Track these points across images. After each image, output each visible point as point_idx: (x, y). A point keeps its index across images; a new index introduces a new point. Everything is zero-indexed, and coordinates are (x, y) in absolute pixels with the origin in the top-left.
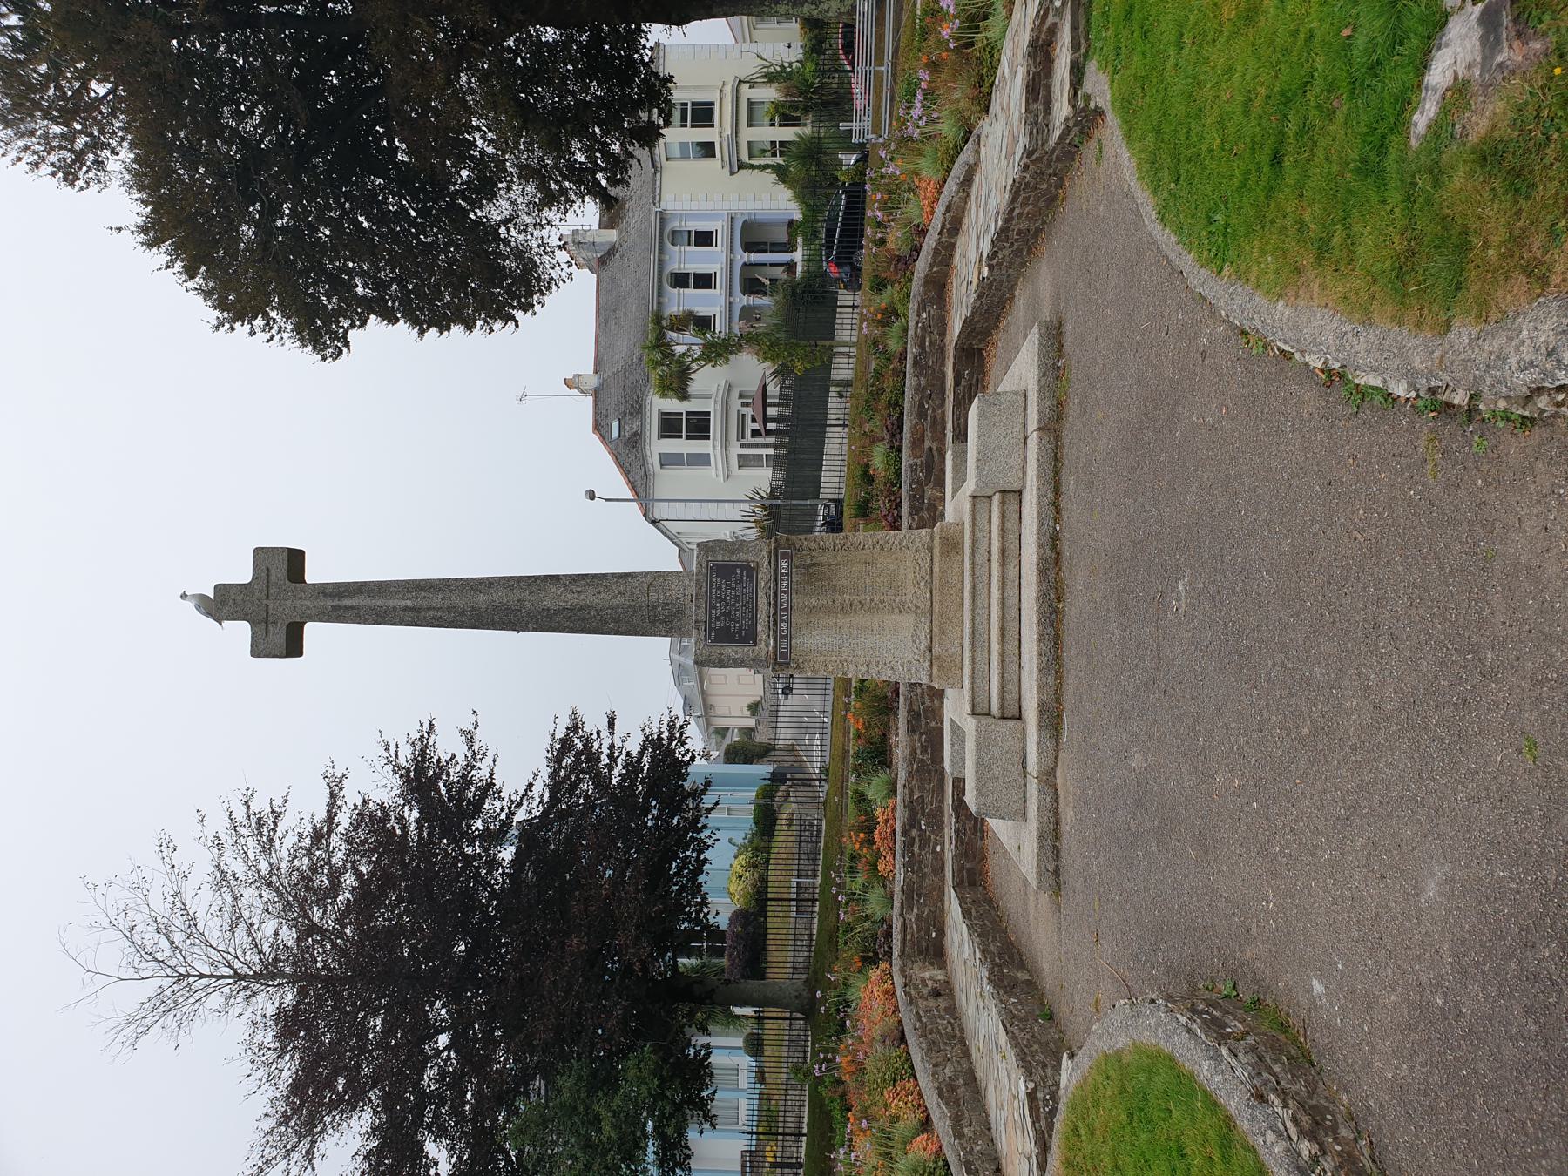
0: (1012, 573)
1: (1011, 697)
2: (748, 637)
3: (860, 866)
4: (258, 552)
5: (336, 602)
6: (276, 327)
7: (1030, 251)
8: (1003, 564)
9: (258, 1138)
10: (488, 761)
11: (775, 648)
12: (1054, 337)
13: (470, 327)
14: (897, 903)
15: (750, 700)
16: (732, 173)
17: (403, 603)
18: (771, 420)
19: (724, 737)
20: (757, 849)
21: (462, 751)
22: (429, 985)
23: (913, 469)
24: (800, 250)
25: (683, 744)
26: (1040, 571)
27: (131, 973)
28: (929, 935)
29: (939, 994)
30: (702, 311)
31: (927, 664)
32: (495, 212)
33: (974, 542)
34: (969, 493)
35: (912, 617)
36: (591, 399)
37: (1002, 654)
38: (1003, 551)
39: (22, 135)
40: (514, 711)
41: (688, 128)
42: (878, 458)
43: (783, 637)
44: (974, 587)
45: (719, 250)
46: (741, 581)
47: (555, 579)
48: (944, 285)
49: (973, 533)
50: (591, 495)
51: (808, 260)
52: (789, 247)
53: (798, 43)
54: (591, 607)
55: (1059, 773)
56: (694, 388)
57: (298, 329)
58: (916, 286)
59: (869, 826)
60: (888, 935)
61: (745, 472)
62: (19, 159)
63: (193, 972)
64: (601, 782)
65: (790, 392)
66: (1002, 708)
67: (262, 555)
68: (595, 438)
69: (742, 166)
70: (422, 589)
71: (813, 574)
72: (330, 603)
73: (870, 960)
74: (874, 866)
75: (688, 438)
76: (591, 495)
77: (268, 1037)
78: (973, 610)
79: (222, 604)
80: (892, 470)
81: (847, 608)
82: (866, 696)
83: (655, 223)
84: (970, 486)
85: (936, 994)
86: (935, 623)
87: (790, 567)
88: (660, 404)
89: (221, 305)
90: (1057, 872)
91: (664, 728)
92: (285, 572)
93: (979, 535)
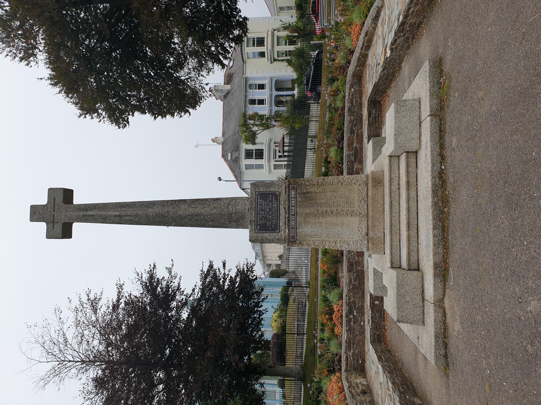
1: (414, 258)
2: (275, 228)
3: (326, 328)
4: (50, 190)
5: (85, 213)
6: (102, 117)
7: (413, 38)
11: (289, 234)
12: (438, 66)
13: (173, 115)
14: (343, 347)
15: (279, 254)
16: (271, 63)
17: (114, 213)
18: (286, 152)
19: (270, 267)
20: (282, 310)
21: (167, 275)
22: (157, 366)
23: (349, 156)
24: (296, 89)
25: (252, 273)
26: (433, 191)
27: (44, 359)
28: (358, 362)
29: (365, 393)
30: (261, 113)
31: (366, 242)
32: (182, 74)
33: (391, 179)
34: (388, 154)
35: (358, 218)
36: (221, 146)
37: (409, 237)
38: (408, 183)
39: (9, 47)
40: (190, 258)
41: (255, 47)
42: (333, 152)
43: (293, 228)
44: (391, 202)
45: (267, 90)
46: (272, 201)
47: (184, 201)
48: (361, 77)
49: (390, 174)
50: (220, 179)
51: (299, 92)
52: (293, 89)
53: (295, 16)
54: (201, 214)
55: (446, 301)
56: (257, 141)
57: (109, 117)
58: (349, 78)
59: (330, 312)
60: (340, 361)
61: (276, 171)
62: (7, 55)
63: (67, 359)
64: (221, 288)
65: (293, 141)
66: (409, 265)
67: (51, 191)
68: (223, 160)
69: (275, 60)
70: (123, 206)
71: (307, 197)
72: (81, 213)
73: (331, 371)
74: (332, 330)
75: (255, 159)
76: (220, 179)
77: (91, 387)
78: (391, 214)
79: (37, 213)
80: (339, 157)
81: (324, 214)
82: (328, 256)
83: (244, 81)
84: (388, 148)
85: (364, 393)
86: (370, 221)
87: (296, 194)
88: (245, 146)
89: (81, 108)
90: (446, 356)
91: (245, 266)
92: (62, 199)
93: (393, 176)
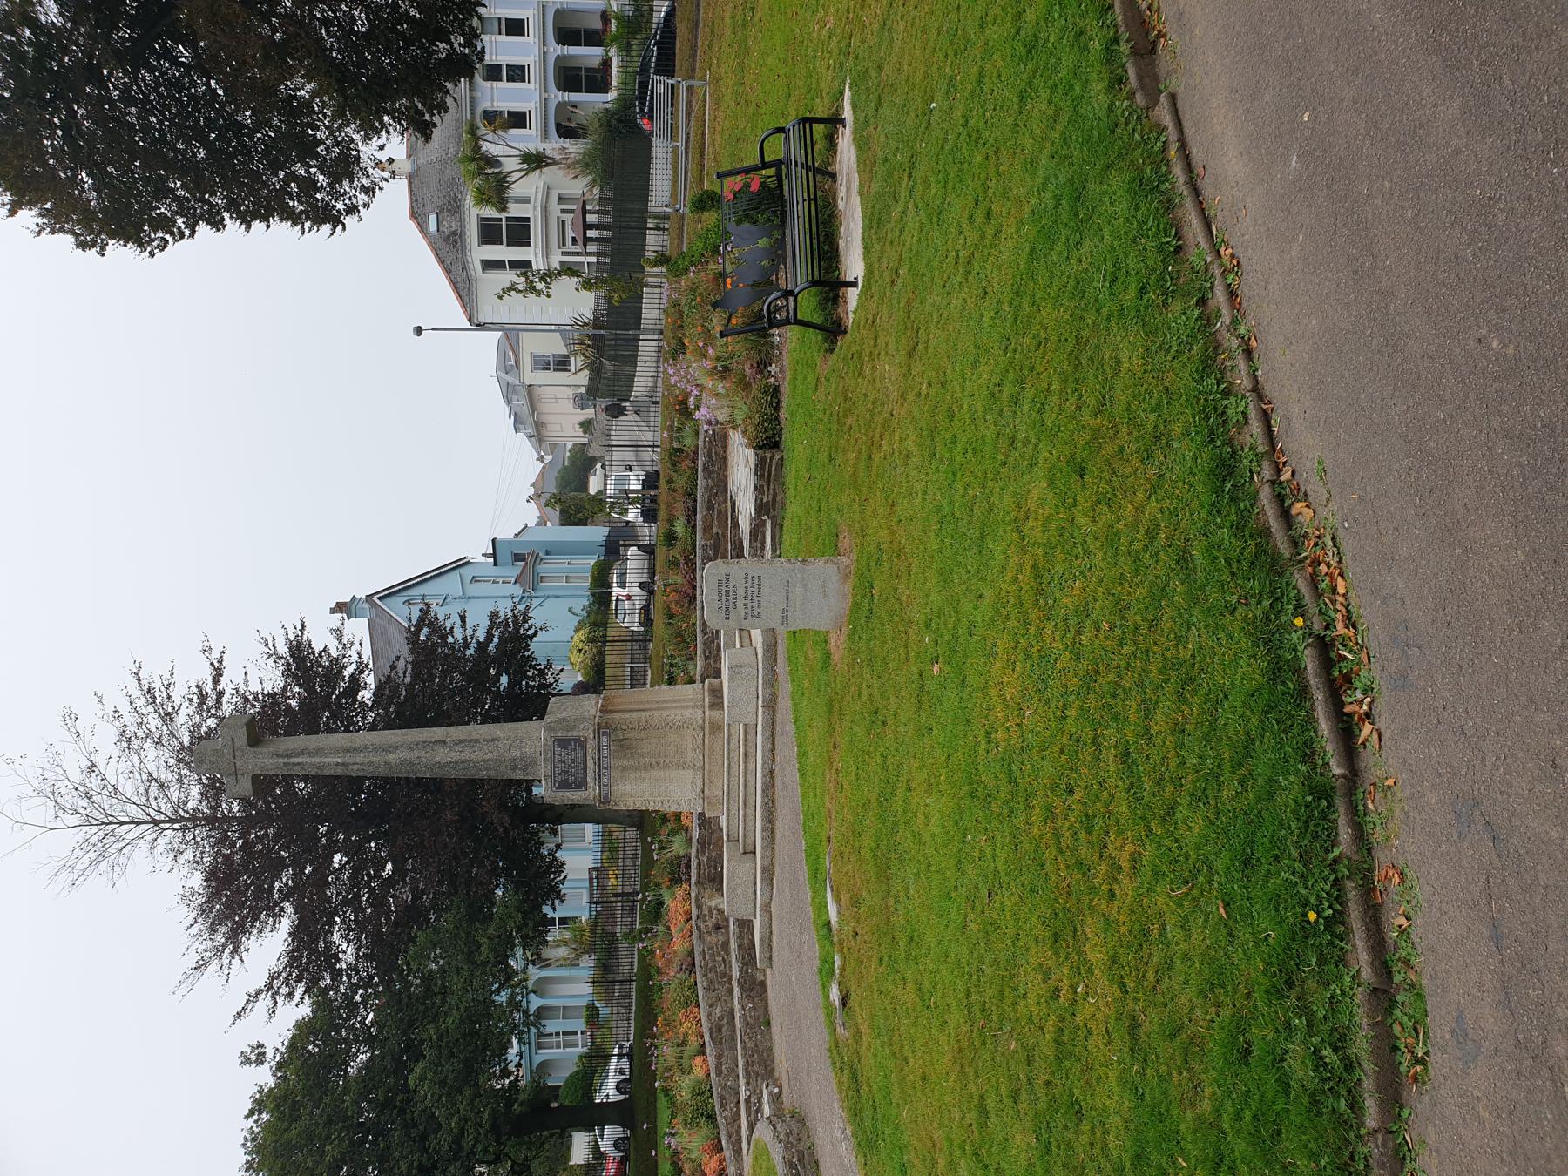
0: (751, 766)
9: (185, 939)
10: (356, 647)
18: (591, 227)
20: (594, 624)
36: (405, 182)
45: (531, 87)
60: (688, 866)
68: (412, 226)
73: (676, 880)
75: (508, 244)
76: (419, 331)
81: (647, 767)
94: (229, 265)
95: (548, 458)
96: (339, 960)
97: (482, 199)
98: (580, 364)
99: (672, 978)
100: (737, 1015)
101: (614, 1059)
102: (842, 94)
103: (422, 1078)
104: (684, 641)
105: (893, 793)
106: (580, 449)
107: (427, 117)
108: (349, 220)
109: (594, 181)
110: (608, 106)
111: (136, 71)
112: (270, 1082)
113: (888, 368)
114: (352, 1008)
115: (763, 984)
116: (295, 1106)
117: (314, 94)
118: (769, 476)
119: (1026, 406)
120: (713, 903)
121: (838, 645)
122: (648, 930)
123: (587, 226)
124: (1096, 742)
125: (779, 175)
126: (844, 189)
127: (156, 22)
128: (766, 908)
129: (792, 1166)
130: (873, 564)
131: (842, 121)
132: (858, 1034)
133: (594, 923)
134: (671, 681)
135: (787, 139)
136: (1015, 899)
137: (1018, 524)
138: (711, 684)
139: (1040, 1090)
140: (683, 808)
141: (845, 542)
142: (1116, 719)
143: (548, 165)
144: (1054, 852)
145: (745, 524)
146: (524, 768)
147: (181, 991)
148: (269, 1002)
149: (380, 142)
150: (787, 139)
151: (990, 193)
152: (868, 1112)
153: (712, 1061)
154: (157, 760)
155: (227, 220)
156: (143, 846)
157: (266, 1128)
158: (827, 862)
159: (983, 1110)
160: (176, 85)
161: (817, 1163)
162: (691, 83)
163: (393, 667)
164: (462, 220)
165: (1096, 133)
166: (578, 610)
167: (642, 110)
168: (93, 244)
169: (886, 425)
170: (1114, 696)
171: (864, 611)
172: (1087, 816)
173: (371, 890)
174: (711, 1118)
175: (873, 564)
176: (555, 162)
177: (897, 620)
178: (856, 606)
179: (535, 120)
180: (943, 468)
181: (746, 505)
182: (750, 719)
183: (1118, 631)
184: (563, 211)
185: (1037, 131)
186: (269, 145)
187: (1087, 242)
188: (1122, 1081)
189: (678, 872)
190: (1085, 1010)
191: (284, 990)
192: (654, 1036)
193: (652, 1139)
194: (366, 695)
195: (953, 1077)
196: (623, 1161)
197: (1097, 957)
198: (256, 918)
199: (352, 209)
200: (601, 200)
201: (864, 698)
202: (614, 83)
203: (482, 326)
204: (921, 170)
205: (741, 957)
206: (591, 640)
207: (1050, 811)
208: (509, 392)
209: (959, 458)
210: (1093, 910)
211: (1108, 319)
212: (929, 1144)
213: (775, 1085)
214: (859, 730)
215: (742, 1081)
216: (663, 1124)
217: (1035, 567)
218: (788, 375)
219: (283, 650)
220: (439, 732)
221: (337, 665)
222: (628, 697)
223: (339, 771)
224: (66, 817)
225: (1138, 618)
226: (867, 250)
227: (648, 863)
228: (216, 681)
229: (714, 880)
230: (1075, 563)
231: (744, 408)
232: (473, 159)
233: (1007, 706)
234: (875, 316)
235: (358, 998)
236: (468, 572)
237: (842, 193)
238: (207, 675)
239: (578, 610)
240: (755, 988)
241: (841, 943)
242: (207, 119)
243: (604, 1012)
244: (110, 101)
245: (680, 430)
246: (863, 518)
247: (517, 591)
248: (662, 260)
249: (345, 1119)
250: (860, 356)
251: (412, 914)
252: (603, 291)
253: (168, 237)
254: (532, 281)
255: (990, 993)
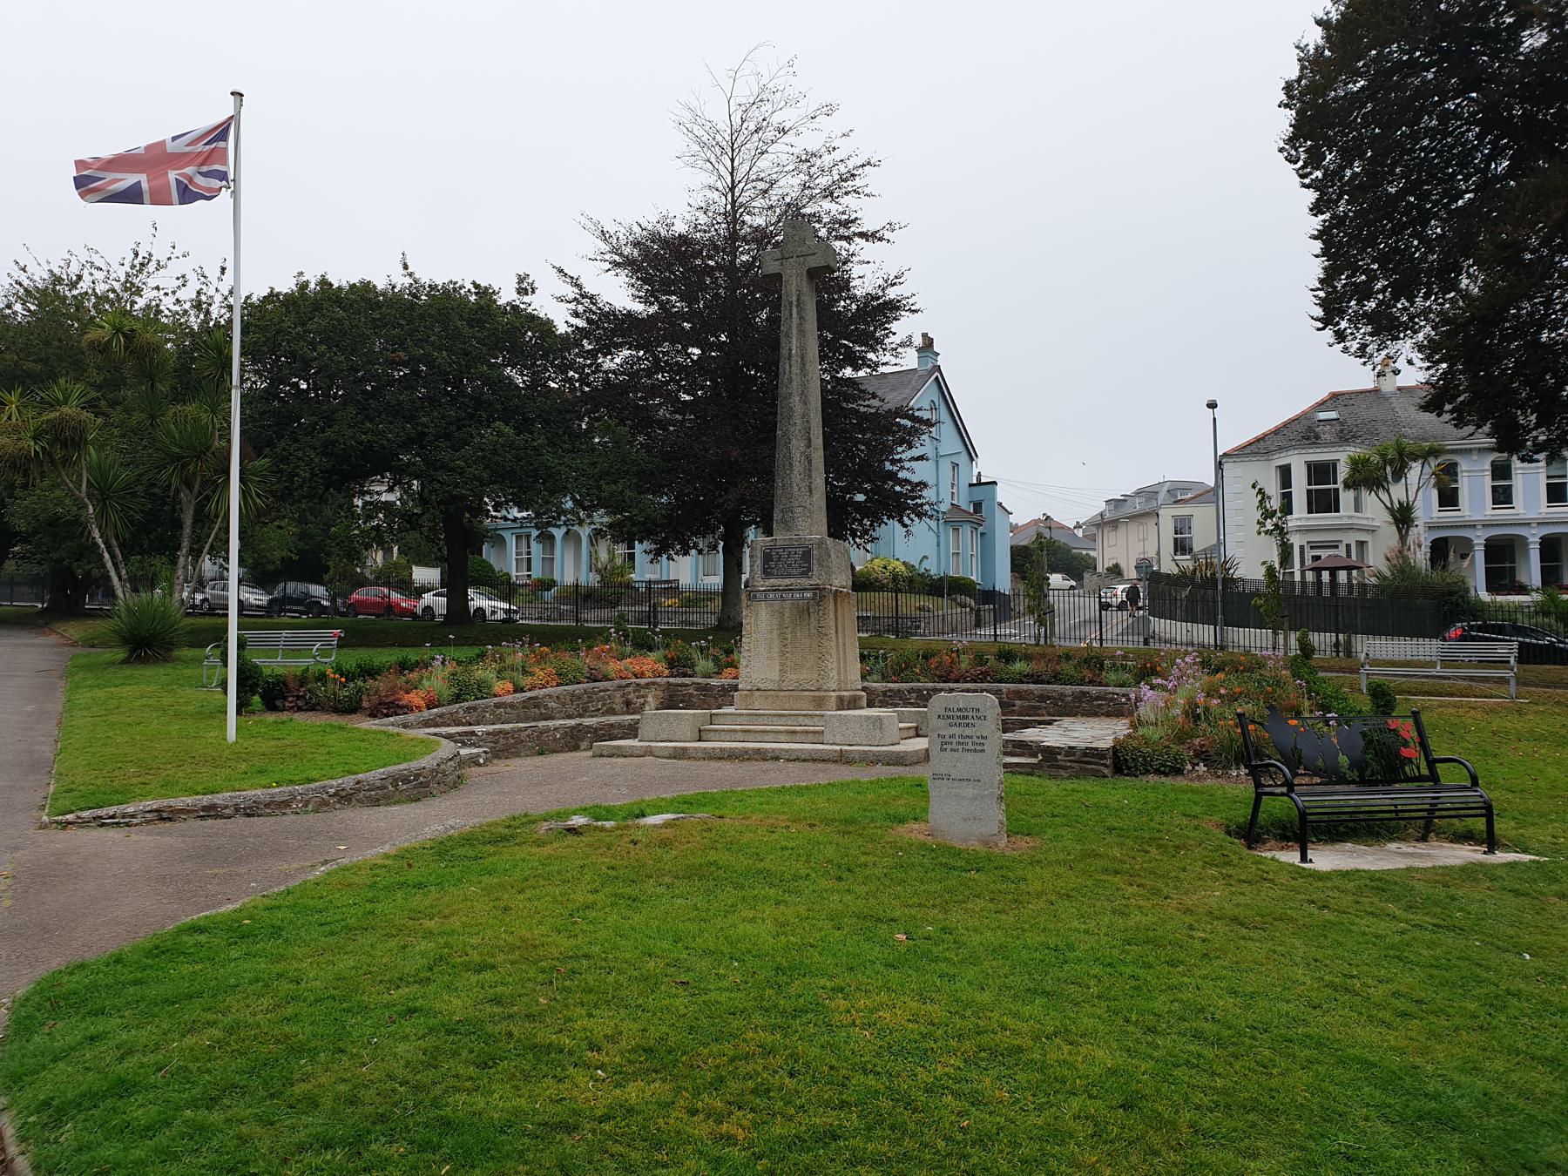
0: (783, 737)
2: (767, 573)
8: (787, 732)
10: (894, 361)
18: (1349, 575)
20: (911, 580)
36: (1371, 386)
38: (794, 732)
45: (1488, 511)
60: (685, 675)
68: (1324, 395)
73: (672, 663)
76: (1212, 405)
94: (1281, 225)
95: (1079, 533)
96: (605, 356)
97: (1356, 464)
98: (1185, 564)
99: (584, 661)
100: (550, 723)
101: (506, 606)
102: (1524, 851)
103: (500, 434)
104: (901, 671)
105: (771, 885)
106: (1090, 565)
107: (1448, 407)
108: (1328, 334)
109: (1385, 578)
110: (1472, 593)
111: (1477, 123)
112: (502, 300)
113: (1215, 895)
114: (563, 369)
115: (576, 748)
116: (480, 323)
117: (1466, 295)
118: (1084, 761)
119: (1191, 1047)
120: (650, 699)
121: (912, 832)
122: (626, 636)
123: (1333, 572)
124: (843, 1105)
125: (1421, 778)
126: (1410, 850)
127: (1530, 141)
128: (649, 752)
129: (417, 776)
130: (1004, 872)
131: (1491, 851)
132: (541, 843)
133: (629, 585)
134: (863, 658)
135: (1465, 788)
136: (682, 1011)
137: (1062, 1033)
138: (860, 697)
139: (503, 1027)
140: (743, 671)
141: (1022, 843)
142: (869, 1129)
143: (1399, 530)
144: (731, 1053)
145: (1030, 735)
146: (783, 520)
147: (583, 220)
148: (571, 296)
149: (1415, 361)
150: (1465, 788)
151: (1433, 1018)
152: (471, 853)
153: (509, 699)
154: (789, 186)
155: (1321, 217)
156: (712, 180)
157: (464, 300)
158: (700, 815)
159: (481, 968)
160: (1465, 160)
161: (418, 800)
162: (1513, 682)
163: (874, 396)
164: (1332, 444)
165: (1519, 1146)
166: (926, 565)
167: (1472, 628)
168: (1290, 97)
169: (1156, 892)
170: (893, 1128)
171: (948, 860)
172: (769, 1090)
173: (667, 383)
174: (458, 698)
175: (1004, 872)
176: (1403, 539)
177: (947, 896)
178: (957, 853)
179: (1449, 515)
180: (1115, 952)
181: (1053, 736)
182: (828, 737)
183: (959, 1137)
184: (1348, 546)
185: (1514, 1077)
186: (1406, 253)
187: (1388, 1129)
188: (517, 1112)
189: (678, 665)
190: (582, 1079)
191: (580, 309)
192: (531, 644)
193: (441, 642)
194: (848, 372)
195: (510, 940)
196: (413, 615)
197: (633, 1092)
198: (645, 281)
199: (1340, 336)
200: (1363, 586)
201: (863, 859)
202: (1499, 598)
203: (1219, 465)
204: (1449, 939)
205: (602, 727)
206: (895, 577)
207: (769, 1051)
208: (1148, 493)
209: (1128, 971)
210: (678, 1091)
211: (1302, 1148)
212: (446, 912)
213: (486, 760)
214: (830, 851)
215: (491, 728)
216: (452, 652)
217: (1020, 1049)
218: (1196, 784)
219: (892, 293)
220: (818, 441)
221: (874, 343)
222: (850, 613)
223: (784, 352)
224: (740, 113)
225: (975, 1160)
226: (1345, 874)
227: (688, 637)
228: (862, 235)
229: (672, 700)
230: (1028, 1094)
231: (1156, 737)
232: (1401, 453)
233: (871, 1012)
234: (1272, 881)
235: (571, 373)
236: (963, 460)
237: (1405, 847)
238: (867, 226)
239: (926, 565)
240: (573, 740)
241: (627, 827)
242: (1429, 193)
243: (548, 596)
244: (1441, 102)
245: (1124, 667)
246: (1050, 863)
247: (944, 507)
248: (1307, 650)
249: (468, 367)
250: (1228, 864)
251: (644, 420)
252: (1263, 589)
253: (1301, 163)
254: (1274, 517)
255: (590, 979)
